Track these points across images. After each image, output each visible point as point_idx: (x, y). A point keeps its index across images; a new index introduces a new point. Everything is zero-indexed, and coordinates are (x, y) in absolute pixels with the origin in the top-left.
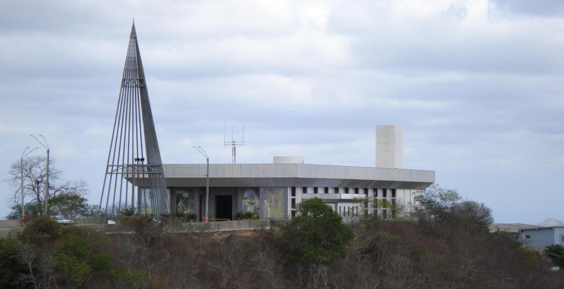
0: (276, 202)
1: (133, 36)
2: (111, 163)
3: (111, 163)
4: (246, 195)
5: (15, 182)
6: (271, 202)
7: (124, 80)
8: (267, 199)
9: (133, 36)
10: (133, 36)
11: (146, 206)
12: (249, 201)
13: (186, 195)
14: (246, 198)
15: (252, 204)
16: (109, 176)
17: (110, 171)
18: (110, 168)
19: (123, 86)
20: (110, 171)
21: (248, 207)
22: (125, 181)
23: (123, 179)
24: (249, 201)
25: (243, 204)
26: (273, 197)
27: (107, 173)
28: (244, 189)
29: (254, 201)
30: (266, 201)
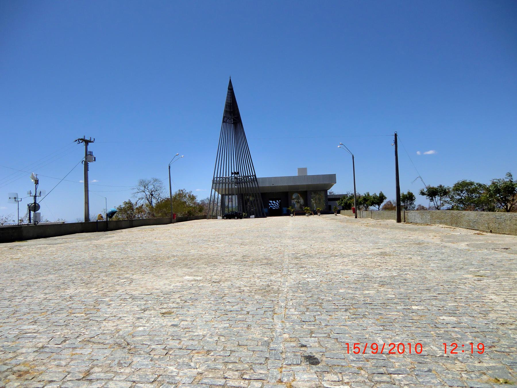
0: (319, 200)
2: (215, 176)
3: (215, 176)
14: (294, 199)
15: (298, 202)
17: (215, 182)
19: (224, 122)
26: (317, 196)
28: (293, 193)
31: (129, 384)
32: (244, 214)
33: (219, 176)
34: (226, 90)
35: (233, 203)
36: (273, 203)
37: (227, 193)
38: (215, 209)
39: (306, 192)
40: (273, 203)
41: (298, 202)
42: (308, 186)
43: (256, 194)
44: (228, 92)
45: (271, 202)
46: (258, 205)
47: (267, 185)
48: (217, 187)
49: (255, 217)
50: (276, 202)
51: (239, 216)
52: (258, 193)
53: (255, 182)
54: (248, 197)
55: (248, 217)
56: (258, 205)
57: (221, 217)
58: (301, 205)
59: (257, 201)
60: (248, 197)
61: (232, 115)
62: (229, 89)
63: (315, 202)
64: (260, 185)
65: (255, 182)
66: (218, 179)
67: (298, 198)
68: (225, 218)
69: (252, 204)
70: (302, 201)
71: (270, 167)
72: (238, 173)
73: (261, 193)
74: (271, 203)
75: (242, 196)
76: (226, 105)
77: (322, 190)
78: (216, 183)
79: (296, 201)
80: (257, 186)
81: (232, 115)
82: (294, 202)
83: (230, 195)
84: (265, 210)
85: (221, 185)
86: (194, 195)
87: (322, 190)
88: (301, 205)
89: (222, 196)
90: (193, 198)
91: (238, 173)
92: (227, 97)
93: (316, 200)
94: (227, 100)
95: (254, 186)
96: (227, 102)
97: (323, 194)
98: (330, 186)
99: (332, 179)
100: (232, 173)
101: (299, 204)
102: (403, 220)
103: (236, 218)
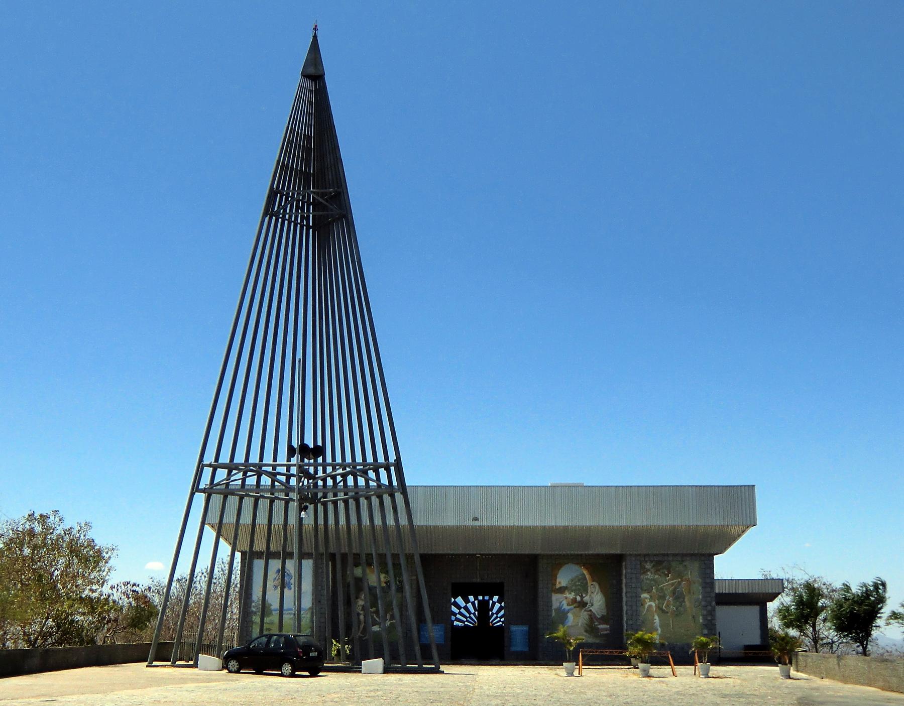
0: (678, 597)
1: (314, 76)
2: (209, 458)
3: (209, 458)
4: (563, 578)
5: (891, 621)
6: (662, 597)
7: (272, 195)
8: (649, 591)
9: (314, 76)
10: (311, 71)
11: (265, 609)
12: (571, 596)
13: (374, 578)
14: (562, 590)
15: (582, 605)
16: (200, 498)
17: (205, 482)
18: (207, 472)
19: (268, 211)
20: (205, 482)
21: (570, 615)
22: (210, 534)
23: (207, 528)
24: (571, 596)
25: (555, 605)
26: (668, 583)
27: (195, 489)
28: (559, 561)
29: (586, 599)
30: (645, 595)
32: (336, 646)
33: (225, 458)
34: (290, 84)
35: (293, 598)
37: (260, 546)
39: (618, 559)
41: (582, 605)
42: (633, 535)
43: (395, 557)
46: (402, 607)
47: (450, 520)
48: (230, 518)
49: (386, 671)
51: (304, 659)
52: (409, 558)
53: (399, 497)
54: (358, 572)
55: (352, 664)
56: (402, 607)
58: (592, 617)
59: (400, 589)
60: (358, 572)
61: (313, 190)
62: (305, 75)
63: (659, 608)
65: (399, 497)
66: (222, 474)
67: (583, 588)
68: (233, 664)
69: (374, 604)
70: (597, 600)
71: (474, 449)
72: (319, 451)
73: (425, 558)
75: (340, 564)
76: (288, 144)
77: (693, 556)
78: (220, 492)
80: (403, 521)
81: (313, 190)
82: (561, 601)
83: (275, 555)
84: (435, 633)
85: (233, 501)
86: (100, 543)
87: (693, 556)
88: (592, 617)
89: (249, 558)
90: (90, 558)
91: (319, 451)
93: (662, 597)
94: (293, 119)
95: (391, 522)
96: (291, 131)
97: (692, 572)
98: (724, 540)
99: (736, 508)
100: (291, 451)
101: (584, 616)
102: (417, 559)
103: (287, 668)
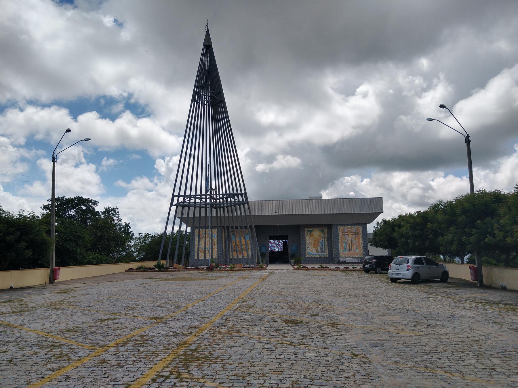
2: (176, 193)
3: (176, 193)
17: (175, 202)
19: (193, 100)
31: (124, 386)
36: (275, 243)
38: (208, 239)
40: (275, 243)
44: (203, 50)
45: (272, 241)
50: (279, 242)
53: (246, 205)
57: (182, 267)
64: (255, 213)
66: (181, 199)
74: (272, 243)
79: (313, 245)
80: (248, 214)
85: (186, 208)
92: (202, 54)
